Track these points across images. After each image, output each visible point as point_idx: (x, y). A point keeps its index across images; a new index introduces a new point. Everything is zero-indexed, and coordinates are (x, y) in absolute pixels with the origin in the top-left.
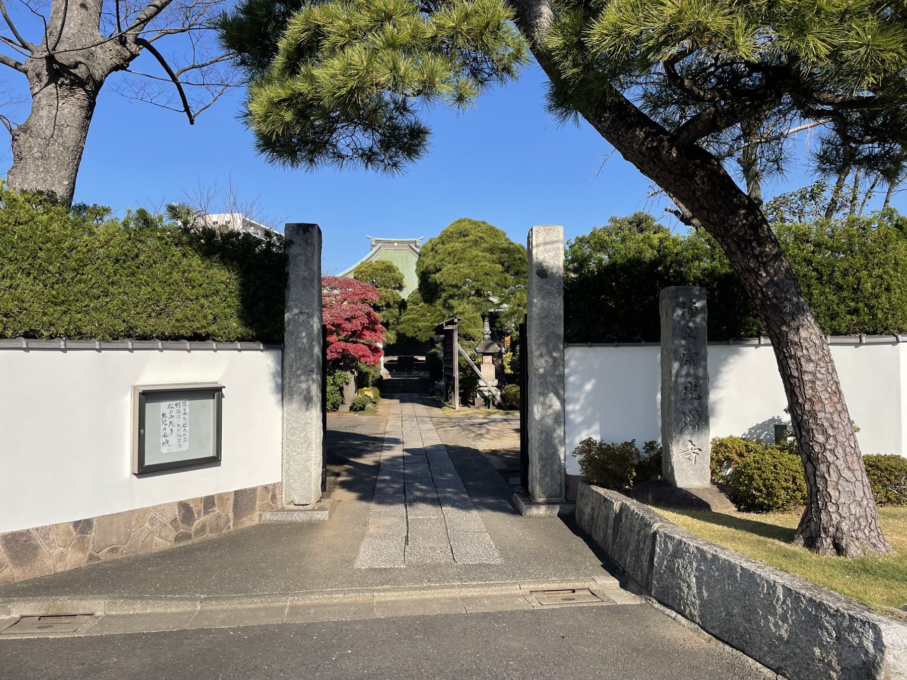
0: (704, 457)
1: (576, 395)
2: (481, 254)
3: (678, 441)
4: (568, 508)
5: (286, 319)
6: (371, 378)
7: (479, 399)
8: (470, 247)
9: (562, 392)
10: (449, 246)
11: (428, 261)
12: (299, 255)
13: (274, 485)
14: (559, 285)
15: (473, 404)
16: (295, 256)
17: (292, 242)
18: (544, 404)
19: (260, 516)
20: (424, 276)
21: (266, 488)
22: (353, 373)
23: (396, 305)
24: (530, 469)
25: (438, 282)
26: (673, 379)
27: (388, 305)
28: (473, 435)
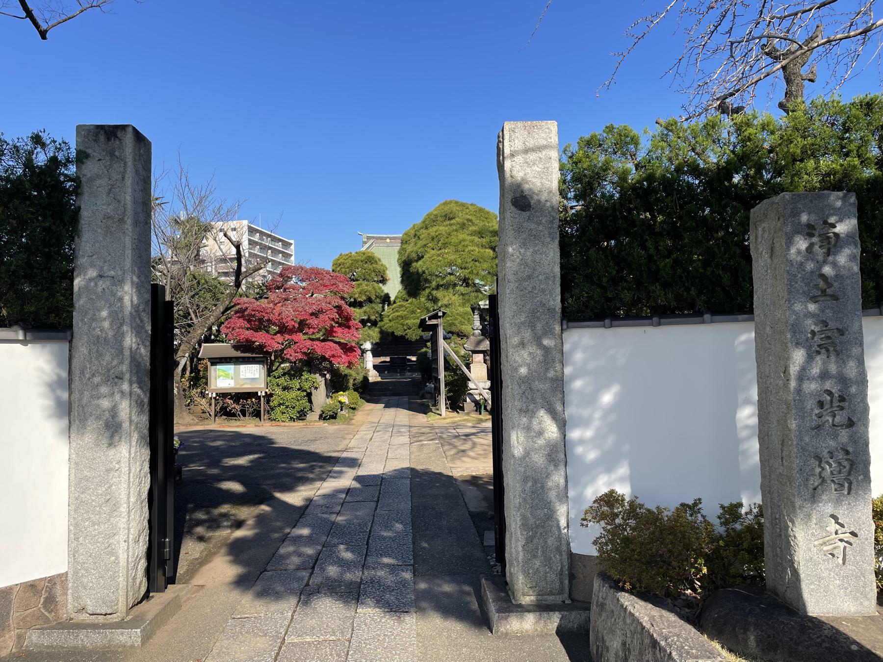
0: (862, 550)
1: (585, 413)
2: (469, 238)
3: (809, 517)
4: (575, 618)
5: (76, 289)
6: (351, 381)
7: (469, 404)
8: (456, 231)
9: (559, 408)
10: (432, 231)
11: (410, 248)
12: (98, 177)
13: (52, 580)
14: (552, 222)
15: (462, 409)
16: (91, 180)
17: (87, 156)
18: (528, 429)
19: (20, 637)
20: (406, 265)
21: (32, 587)
22: (324, 376)
23: (378, 300)
24: (507, 541)
25: (420, 271)
26: (793, 384)
27: (370, 300)
28: (453, 452)
